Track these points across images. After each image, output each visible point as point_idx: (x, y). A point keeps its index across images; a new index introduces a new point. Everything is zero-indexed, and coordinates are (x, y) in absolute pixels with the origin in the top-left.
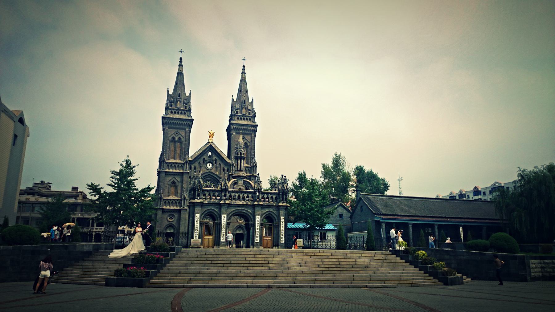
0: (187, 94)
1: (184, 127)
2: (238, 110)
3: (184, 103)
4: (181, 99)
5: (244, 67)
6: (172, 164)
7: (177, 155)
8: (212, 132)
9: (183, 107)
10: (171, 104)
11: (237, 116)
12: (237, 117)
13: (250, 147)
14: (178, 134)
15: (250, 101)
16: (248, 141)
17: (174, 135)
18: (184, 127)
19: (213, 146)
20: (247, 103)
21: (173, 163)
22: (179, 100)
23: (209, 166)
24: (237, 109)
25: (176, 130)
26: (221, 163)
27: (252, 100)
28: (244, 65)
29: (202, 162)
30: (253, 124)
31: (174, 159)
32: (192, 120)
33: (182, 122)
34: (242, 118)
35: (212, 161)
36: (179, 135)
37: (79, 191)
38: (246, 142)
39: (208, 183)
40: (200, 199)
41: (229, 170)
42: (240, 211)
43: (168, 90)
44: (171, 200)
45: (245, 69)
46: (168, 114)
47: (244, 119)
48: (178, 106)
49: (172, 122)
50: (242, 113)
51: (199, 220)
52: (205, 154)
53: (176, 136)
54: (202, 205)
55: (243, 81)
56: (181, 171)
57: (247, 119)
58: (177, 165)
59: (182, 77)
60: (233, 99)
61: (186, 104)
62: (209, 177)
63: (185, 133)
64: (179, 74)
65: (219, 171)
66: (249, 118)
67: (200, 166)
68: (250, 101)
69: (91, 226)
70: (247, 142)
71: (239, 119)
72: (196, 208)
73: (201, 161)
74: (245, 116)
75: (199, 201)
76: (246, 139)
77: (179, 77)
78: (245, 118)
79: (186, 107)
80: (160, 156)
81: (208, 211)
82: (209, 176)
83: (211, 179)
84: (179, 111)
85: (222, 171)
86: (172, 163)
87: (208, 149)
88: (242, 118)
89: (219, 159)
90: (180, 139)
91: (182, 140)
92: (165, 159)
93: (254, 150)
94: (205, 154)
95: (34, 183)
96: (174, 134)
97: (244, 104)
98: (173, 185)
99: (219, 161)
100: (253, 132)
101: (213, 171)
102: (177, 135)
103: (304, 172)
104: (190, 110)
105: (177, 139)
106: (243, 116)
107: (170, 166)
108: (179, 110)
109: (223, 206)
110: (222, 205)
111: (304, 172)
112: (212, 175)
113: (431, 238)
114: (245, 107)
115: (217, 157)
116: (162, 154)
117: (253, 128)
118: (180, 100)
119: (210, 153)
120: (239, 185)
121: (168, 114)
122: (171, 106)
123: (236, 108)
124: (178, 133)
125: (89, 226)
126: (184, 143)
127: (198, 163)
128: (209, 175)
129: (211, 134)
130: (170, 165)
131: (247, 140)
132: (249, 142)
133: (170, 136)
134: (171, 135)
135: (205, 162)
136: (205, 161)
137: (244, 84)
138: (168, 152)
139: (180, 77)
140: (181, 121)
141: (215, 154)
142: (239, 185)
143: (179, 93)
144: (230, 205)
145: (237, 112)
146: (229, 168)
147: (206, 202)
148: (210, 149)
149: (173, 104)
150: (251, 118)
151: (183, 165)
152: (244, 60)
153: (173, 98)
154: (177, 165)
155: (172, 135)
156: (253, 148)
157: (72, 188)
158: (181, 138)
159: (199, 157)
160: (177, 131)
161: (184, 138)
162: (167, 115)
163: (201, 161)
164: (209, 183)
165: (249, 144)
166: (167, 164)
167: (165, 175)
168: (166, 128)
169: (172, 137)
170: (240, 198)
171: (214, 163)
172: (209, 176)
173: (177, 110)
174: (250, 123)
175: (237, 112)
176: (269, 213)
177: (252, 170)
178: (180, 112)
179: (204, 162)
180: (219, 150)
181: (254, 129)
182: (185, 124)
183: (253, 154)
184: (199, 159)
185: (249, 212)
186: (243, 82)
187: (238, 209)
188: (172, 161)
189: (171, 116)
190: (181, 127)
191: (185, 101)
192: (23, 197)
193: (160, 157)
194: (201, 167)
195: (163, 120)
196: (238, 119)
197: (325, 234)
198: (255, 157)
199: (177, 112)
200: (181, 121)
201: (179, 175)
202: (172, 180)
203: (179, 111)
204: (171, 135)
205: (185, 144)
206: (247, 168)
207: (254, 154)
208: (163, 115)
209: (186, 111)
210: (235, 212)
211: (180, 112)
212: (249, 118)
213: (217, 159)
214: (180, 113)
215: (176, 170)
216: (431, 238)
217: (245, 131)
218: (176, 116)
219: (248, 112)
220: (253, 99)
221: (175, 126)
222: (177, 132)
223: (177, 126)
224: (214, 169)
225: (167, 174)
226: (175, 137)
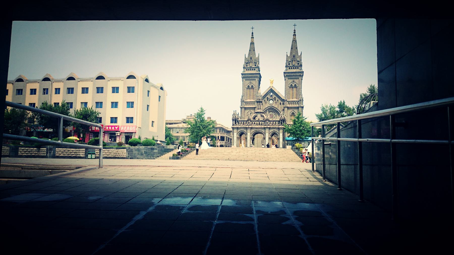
1: (254, 78)
2: (290, 63)
3: (254, 63)
4: (295, 59)
5: (295, 31)
8: (272, 80)
9: (296, 64)
11: (288, 67)
12: (289, 67)
13: (298, 87)
14: (251, 83)
15: (299, 54)
16: (296, 83)
17: (249, 85)
20: (297, 56)
25: (249, 81)
27: (300, 53)
28: (295, 29)
29: (266, 100)
30: (300, 71)
31: (250, 99)
32: (303, 72)
33: (253, 75)
34: (293, 67)
35: (272, 99)
38: (295, 84)
41: (284, 104)
45: (295, 32)
46: (245, 71)
47: (294, 68)
51: (236, 136)
56: (297, 106)
59: (253, 45)
60: (287, 55)
62: (271, 109)
63: (255, 83)
65: (278, 105)
66: (297, 67)
67: (265, 103)
68: (299, 54)
70: (296, 84)
71: (291, 68)
72: (234, 130)
77: (251, 46)
78: (295, 67)
79: (255, 66)
80: (241, 98)
81: (241, 132)
82: (271, 108)
83: (272, 110)
84: (251, 69)
85: (279, 105)
88: (293, 67)
89: (277, 97)
90: (252, 86)
91: (254, 87)
92: (244, 100)
93: (301, 89)
94: (268, 94)
96: (249, 83)
97: (294, 58)
99: (277, 99)
101: (273, 105)
102: (250, 84)
103: (344, 101)
104: (301, 66)
109: (234, 129)
111: (344, 101)
112: (273, 108)
114: (295, 59)
115: (276, 96)
117: (300, 74)
118: (252, 61)
119: (271, 94)
121: (245, 71)
123: (289, 61)
126: (255, 88)
129: (272, 81)
131: (296, 83)
132: (297, 84)
135: (269, 100)
136: (268, 99)
137: (294, 43)
138: (246, 95)
139: (252, 45)
141: (275, 94)
144: (251, 128)
145: (289, 64)
146: (284, 103)
147: (240, 127)
148: (271, 91)
149: (247, 64)
150: (255, 68)
151: (298, 102)
152: (295, 25)
153: (248, 61)
155: (248, 84)
156: (300, 88)
159: (264, 97)
161: (254, 85)
164: (272, 113)
165: (297, 85)
167: (245, 109)
168: (287, 79)
171: (274, 100)
172: (271, 108)
173: (250, 68)
176: (274, 132)
178: (252, 69)
179: (268, 100)
181: (301, 75)
182: (255, 76)
183: (300, 91)
185: (263, 132)
186: (294, 42)
187: (257, 130)
188: (248, 100)
190: (253, 79)
192: (226, 127)
194: (266, 103)
195: (285, 74)
196: (289, 68)
198: (302, 93)
202: (292, 112)
203: (251, 69)
205: (256, 89)
207: (301, 92)
211: (252, 69)
212: (297, 67)
213: (276, 97)
214: (252, 70)
215: (251, 106)
220: (301, 53)
221: (249, 79)
222: (250, 82)
224: (275, 103)
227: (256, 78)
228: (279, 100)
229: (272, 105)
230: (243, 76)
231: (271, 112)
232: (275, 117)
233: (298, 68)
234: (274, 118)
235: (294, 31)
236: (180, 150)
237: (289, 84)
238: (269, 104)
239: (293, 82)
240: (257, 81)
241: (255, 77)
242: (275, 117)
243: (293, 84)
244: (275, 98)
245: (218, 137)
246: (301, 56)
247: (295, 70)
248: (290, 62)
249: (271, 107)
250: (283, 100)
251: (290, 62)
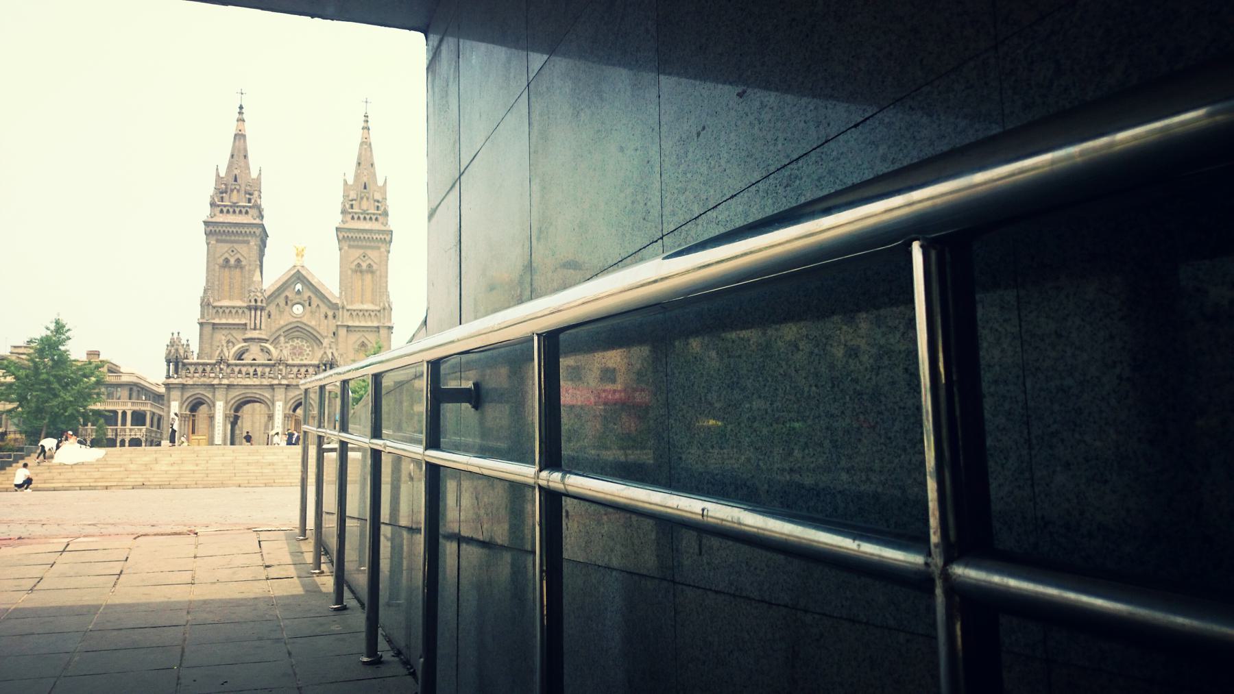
0: (254, 175)
1: (246, 238)
2: (354, 202)
3: (246, 193)
6: (225, 309)
7: (368, 294)
9: (244, 200)
10: (221, 195)
11: (350, 213)
17: (227, 255)
18: (246, 238)
19: (304, 273)
22: (235, 188)
23: (298, 309)
24: (352, 200)
25: (229, 245)
26: (320, 305)
29: (282, 303)
30: (383, 228)
31: (231, 298)
35: (302, 302)
36: (367, 259)
37: (101, 358)
40: (178, 377)
42: (248, 395)
43: (217, 169)
46: (215, 215)
48: (234, 199)
49: (222, 231)
50: (360, 209)
52: (289, 289)
53: (232, 256)
54: (183, 387)
55: (366, 144)
56: (376, 324)
58: (356, 313)
61: (250, 194)
62: (298, 331)
64: (237, 137)
69: (122, 426)
70: (372, 263)
72: (172, 393)
73: (281, 301)
74: (368, 214)
75: (176, 381)
76: (370, 258)
77: (237, 141)
78: (368, 217)
81: (193, 398)
86: (224, 307)
87: (293, 279)
88: (362, 217)
90: (238, 261)
91: (243, 263)
95: (12, 346)
96: (227, 252)
97: (365, 191)
98: (363, 348)
99: (315, 301)
100: (252, 237)
101: (305, 320)
104: (386, 214)
105: (232, 261)
106: (362, 214)
107: (354, 316)
108: (235, 206)
110: (216, 386)
114: (367, 195)
116: (205, 291)
118: (238, 187)
119: (299, 286)
120: (252, 354)
122: (222, 199)
125: (117, 425)
126: (247, 268)
127: (274, 306)
128: (298, 327)
130: (354, 314)
131: (371, 259)
133: (219, 258)
134: (222, 256)
136: (289, 302)
140: (239, 228)
142: (252, 354)
143: (234, 173)
145: (352, 206)
146: (337, 314)
148: (299, 278)
150: (378, 216)
151: (378, 314)
153: (225, 184)
154: (356, 313)
157: (87, 354)
158: (242, 259)
159: (277, 293)
160: (233, 247)
161: (246, 258)
162: (212, 217)
163: (281, 301)
164: (299, 341)
166: (349, 313)
167: (213, 328)
169: (223, 258)
170: (257, 374)
171: (307, 304)
173: (231, 206)
174: (375, 226)
175: (352, 206)
177: (382, 316)
178: (237, 210)
183: (384, 285)
184: (276, 297)
193: (204, 297)
194: (281, 312)
199: (231, 210)
200: (239, 228)
201: (371, 331)
204: (222, 256)
206: (373, 311)
207: (387, 286)
208: (206, 217)
209: (250, 207)
210: (241, 397)
211: (237, 210)
213: (313, 296)
214: (237, 212)
217: (366, 242)
218: (231, 218)
219: (374, 205)
220: (386, 179)
221: (228, 238)
223: (233, 238)
225: (351, 331)
228: (322, 305)
229: (299, 320)
230: (211, 228)
231: (298, 338)
233: (247, 213)
234: (306, 357)
235: (238, 110)
237: (352, 263)
239: (362, 258)
240: (255, 247)
242: (308, 355)
245: (124, 413)
248: (355, 200)
250: (334, 307)
251: (355, 200)
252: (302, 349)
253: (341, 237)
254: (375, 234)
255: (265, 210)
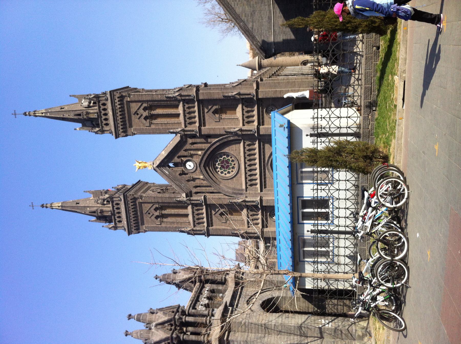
12: (104, 126)
17: (153, 218)
21: (194, 217)
23: (190, 165)
25: (133, 117)
39: (217, 166)
44: (243, 115)
57: (105, 110)
78: (103, 112)
113: (322, 33)
124: (148, 213)
132: (141, 105)
165: (145, 105)
180: (163, 152)
181: (118, 98)
189: (125, 222)
191: (99, 202)
197: (306, 204)
203: (116, 212)
214: (119, 211)
216: (322, 33)
226: (154, 216)
227: (125, 102)
229: (198, 165)
230: (133, 230)
232: (233, 161)
233: (118, 204)
236: (412, 295)
238: (197, 171)
241: (122, 104)
243: (142, 115)
244: (179, 157)
246: (79, 96)
247: (109, 110)
249: (202, 165)
252: (223, 160)
253: (123, 134)
254: (115, 106)
255: (103, 92)
